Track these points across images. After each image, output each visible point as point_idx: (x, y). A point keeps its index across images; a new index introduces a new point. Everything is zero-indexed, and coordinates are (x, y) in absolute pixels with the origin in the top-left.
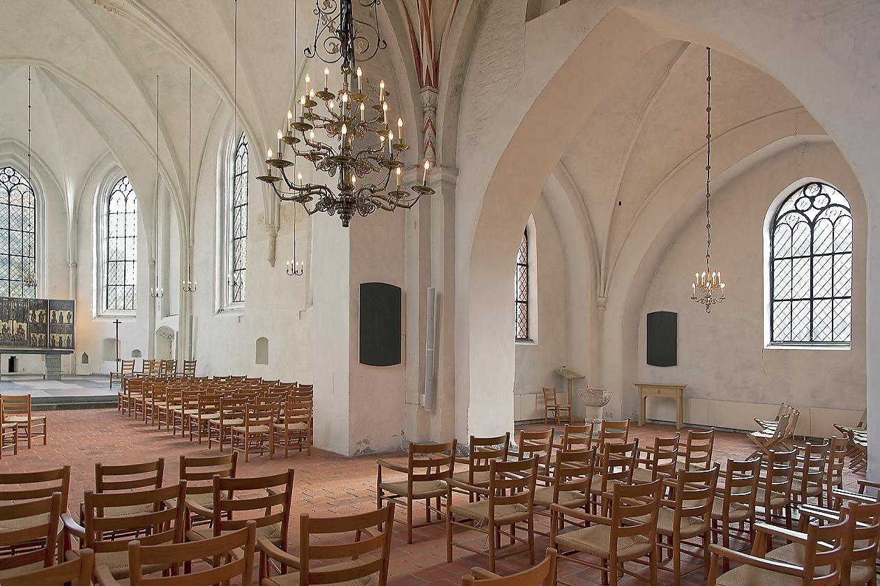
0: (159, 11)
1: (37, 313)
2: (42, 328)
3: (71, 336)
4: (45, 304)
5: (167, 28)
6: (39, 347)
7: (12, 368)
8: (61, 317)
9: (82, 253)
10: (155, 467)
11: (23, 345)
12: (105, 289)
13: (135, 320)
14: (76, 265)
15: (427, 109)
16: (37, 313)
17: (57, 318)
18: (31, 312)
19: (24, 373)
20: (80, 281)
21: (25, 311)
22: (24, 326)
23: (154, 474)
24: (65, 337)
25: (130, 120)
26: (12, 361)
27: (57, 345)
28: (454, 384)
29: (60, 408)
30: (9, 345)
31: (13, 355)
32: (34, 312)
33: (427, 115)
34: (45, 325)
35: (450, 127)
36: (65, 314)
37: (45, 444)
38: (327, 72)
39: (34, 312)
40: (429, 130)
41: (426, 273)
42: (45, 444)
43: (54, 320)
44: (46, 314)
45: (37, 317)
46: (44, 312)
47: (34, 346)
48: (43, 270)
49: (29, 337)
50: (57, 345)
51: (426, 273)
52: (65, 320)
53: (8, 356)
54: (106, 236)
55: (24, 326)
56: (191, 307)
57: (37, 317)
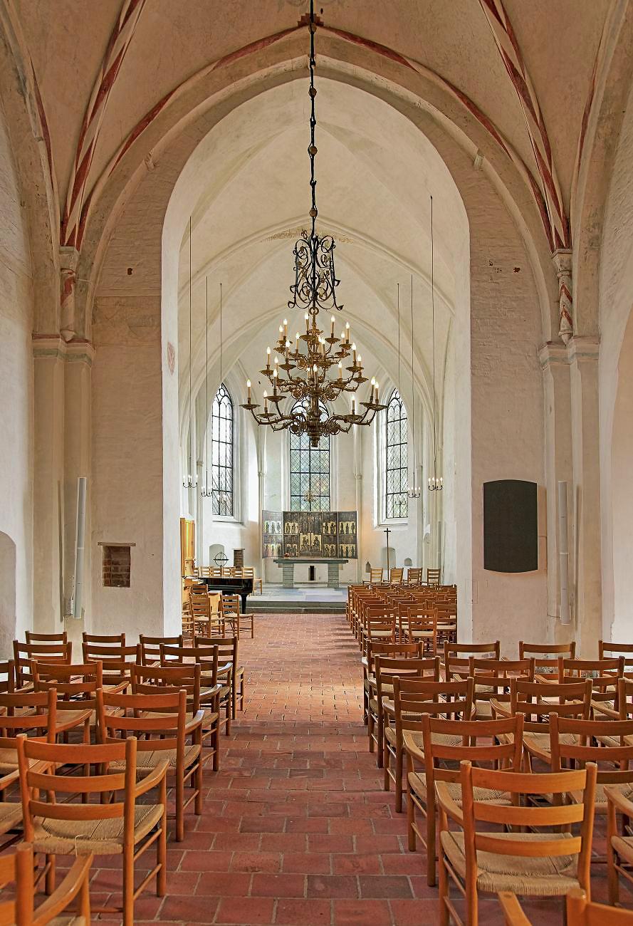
0: (370, 233)
1: (329, 525)
2: (334, 539)
3: (354, 546)
4: (336, 517)
5: (377, 245)
6: (332, 556)
7: (312, 578)
8: (347, 527)
9: (366, 464)
10: (231, 642)
11: (318, 555)
12: (385, 498)
13: (406, 528)
14: (361, 477)
15: (559, 275)
16: (329, 525)
17: (345, 529)
18: (324, 524)
19: (320, 581)
20: (364, 492)
21: (320, 524)
22: (320, 537)
23: (231, 647)
24: (350, 546)
25: (381, 332)
26: (312, 569)
27: (344, 555)
28: (600, 594)
29: (307, 612)
30: (308, 555)
31: (312, 565)
32: (326, 524)
33: (560, 281)
34: (335, 536)
35: (587, 289)
36: (350, 524)
37: (252, 638)
38: (333, 319)
39: (326, 524)
40: (564, 298)
41: (565, 462)
42: (252, 638)
43: (342, 531)
44: (336, 526)
45: (329, 529)
46: (335, 524)
47: (328, 556)
48: (336, 485)
49: (323, 547)
50: (344, 555)
51: (565, 462)
52: (350, 532)
53: (309, 565)
54: (385, 445)
55: (320, 537)
56: (441, 513)
57: (329, 529)
